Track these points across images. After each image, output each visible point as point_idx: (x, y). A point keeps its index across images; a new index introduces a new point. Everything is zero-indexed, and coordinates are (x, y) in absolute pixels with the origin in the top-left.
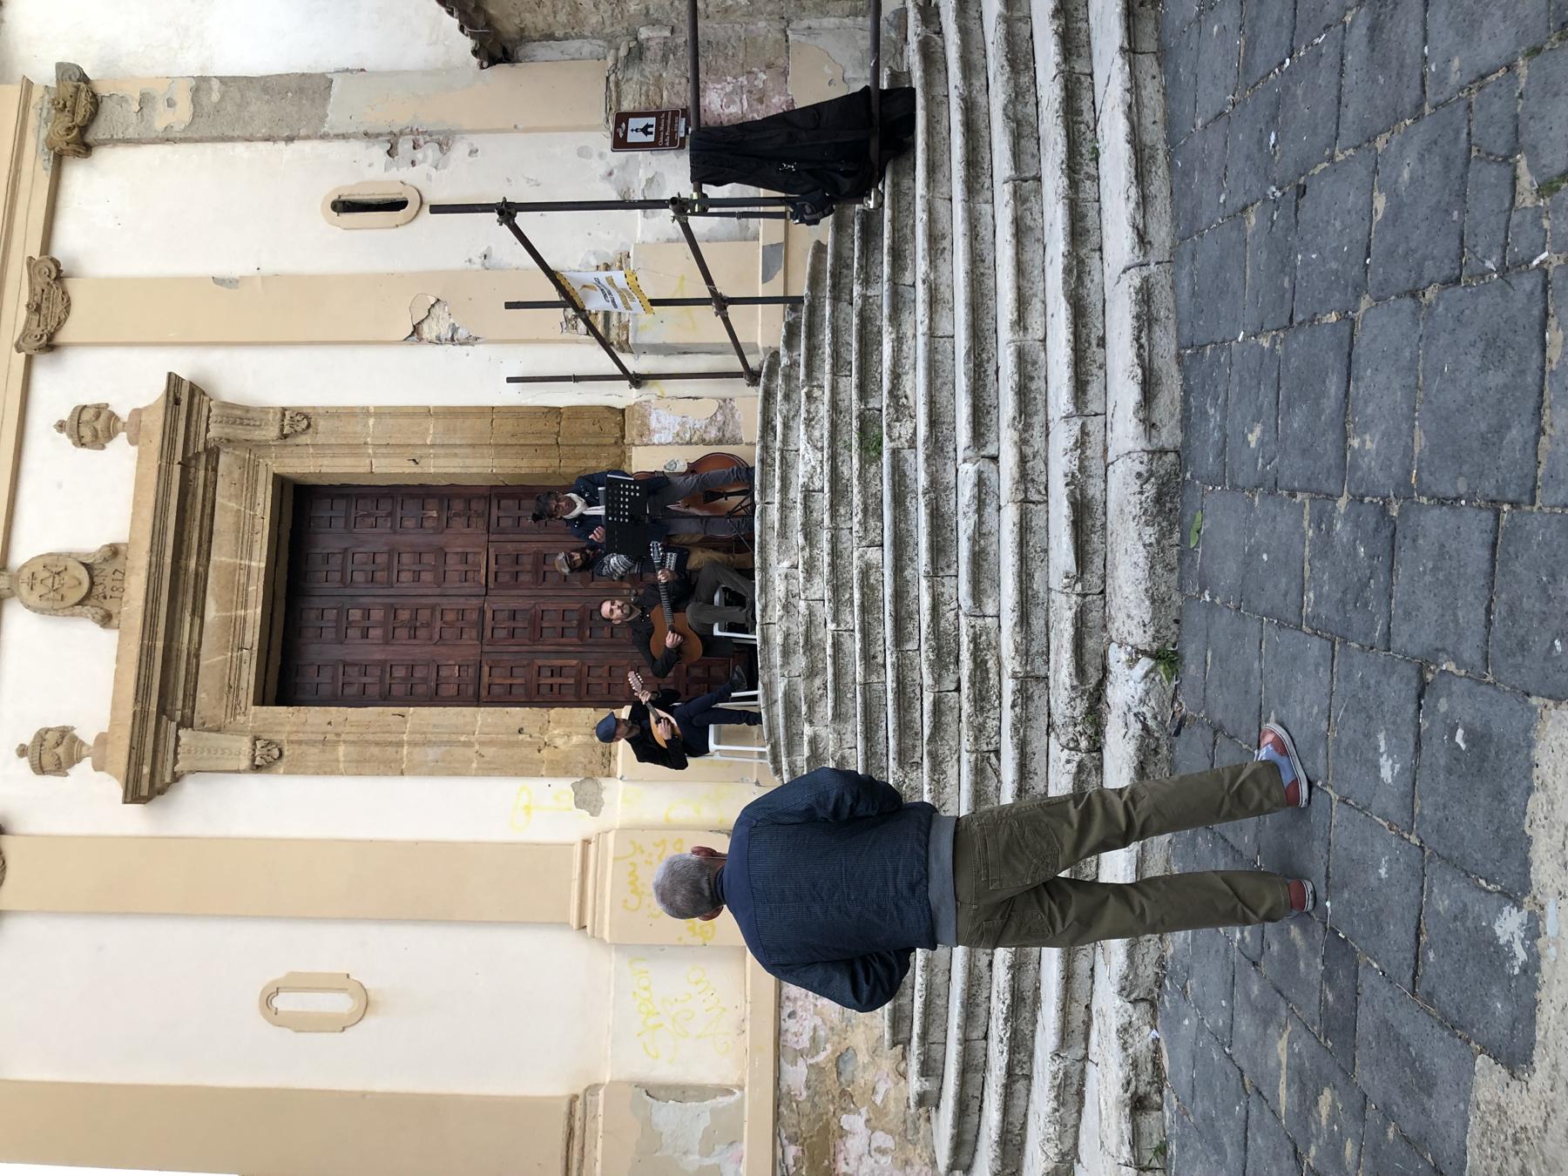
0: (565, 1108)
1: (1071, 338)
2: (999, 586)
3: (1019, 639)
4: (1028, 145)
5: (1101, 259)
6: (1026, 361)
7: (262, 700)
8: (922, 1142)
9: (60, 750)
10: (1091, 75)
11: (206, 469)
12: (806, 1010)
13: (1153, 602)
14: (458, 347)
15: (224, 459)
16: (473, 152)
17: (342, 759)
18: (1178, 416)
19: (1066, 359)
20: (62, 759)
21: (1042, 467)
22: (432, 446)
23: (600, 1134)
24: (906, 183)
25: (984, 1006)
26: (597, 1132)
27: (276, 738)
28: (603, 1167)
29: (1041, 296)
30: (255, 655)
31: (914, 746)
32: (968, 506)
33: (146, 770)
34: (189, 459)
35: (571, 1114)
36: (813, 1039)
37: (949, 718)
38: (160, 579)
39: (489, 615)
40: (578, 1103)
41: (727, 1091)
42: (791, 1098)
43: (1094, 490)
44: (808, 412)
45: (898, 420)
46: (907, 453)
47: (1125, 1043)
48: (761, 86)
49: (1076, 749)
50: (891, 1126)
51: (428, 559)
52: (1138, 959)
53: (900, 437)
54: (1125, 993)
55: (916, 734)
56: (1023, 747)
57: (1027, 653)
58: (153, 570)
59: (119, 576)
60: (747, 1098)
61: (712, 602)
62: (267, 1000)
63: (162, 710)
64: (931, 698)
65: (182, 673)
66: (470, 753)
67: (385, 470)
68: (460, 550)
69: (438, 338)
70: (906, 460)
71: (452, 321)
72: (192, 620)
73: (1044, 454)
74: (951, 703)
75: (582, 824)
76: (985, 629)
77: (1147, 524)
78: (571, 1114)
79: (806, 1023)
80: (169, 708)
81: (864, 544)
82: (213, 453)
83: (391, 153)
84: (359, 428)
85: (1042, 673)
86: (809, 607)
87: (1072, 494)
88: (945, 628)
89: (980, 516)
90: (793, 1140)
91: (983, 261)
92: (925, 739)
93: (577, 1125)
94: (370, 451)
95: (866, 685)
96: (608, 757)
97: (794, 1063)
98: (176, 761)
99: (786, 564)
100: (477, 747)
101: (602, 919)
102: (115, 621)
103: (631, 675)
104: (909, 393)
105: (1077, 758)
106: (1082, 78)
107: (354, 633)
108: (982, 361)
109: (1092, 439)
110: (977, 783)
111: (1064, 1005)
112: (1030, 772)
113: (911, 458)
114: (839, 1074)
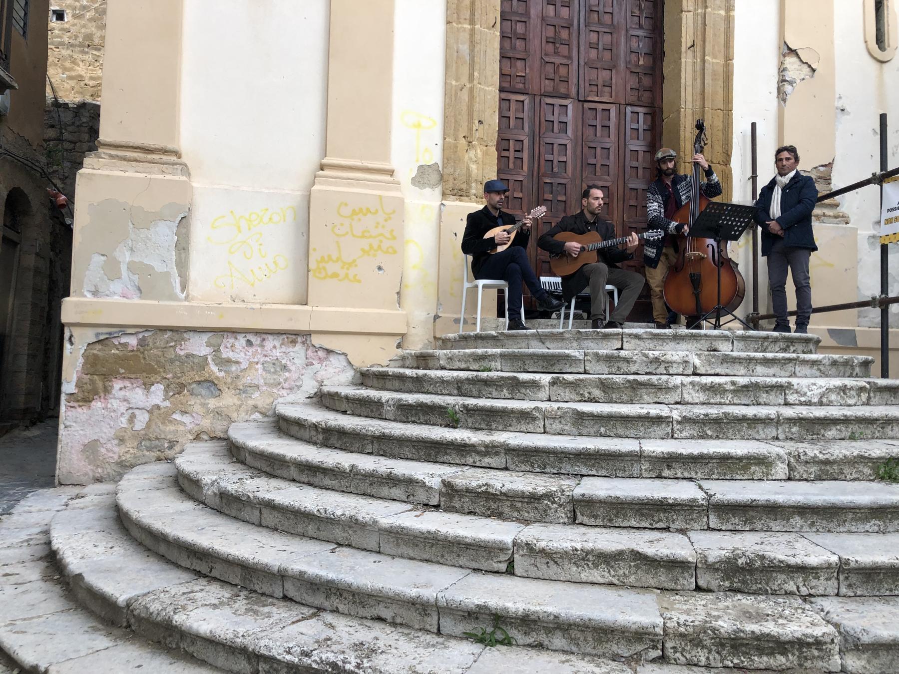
0: (170, 146)
8: (140, 453)
12: (254, 355)
14: (776, 86)
22: (704, 61)
23: (149, 176)
25: (326, 604)
26: (150, 173)
28: (119, 177)
36: (229, 361)
39: (564, 102)
40: (175, 158)
41: (184, 287)
42: (179, 342)
44: (851, 388)
50: (153, 427)
60: (179, 303)
61: (608, 284)
66: (464, 80)
67: (684, 21)
68: (614, 81)
69: (785, 70)
71: (798, 81)
74: (682, 581)
78: (165, 152)
79: (242, 354)
81: (792, 460)
86: (675, 387)
88: (775, 579)
90: (142, 343)
93: (156, 157)
94: (700, 11)
96: (461, 194)
97: (208, 345)
100: (468, 86)
101: (330, 184)
110: (623, 632)
114: (199, 383)
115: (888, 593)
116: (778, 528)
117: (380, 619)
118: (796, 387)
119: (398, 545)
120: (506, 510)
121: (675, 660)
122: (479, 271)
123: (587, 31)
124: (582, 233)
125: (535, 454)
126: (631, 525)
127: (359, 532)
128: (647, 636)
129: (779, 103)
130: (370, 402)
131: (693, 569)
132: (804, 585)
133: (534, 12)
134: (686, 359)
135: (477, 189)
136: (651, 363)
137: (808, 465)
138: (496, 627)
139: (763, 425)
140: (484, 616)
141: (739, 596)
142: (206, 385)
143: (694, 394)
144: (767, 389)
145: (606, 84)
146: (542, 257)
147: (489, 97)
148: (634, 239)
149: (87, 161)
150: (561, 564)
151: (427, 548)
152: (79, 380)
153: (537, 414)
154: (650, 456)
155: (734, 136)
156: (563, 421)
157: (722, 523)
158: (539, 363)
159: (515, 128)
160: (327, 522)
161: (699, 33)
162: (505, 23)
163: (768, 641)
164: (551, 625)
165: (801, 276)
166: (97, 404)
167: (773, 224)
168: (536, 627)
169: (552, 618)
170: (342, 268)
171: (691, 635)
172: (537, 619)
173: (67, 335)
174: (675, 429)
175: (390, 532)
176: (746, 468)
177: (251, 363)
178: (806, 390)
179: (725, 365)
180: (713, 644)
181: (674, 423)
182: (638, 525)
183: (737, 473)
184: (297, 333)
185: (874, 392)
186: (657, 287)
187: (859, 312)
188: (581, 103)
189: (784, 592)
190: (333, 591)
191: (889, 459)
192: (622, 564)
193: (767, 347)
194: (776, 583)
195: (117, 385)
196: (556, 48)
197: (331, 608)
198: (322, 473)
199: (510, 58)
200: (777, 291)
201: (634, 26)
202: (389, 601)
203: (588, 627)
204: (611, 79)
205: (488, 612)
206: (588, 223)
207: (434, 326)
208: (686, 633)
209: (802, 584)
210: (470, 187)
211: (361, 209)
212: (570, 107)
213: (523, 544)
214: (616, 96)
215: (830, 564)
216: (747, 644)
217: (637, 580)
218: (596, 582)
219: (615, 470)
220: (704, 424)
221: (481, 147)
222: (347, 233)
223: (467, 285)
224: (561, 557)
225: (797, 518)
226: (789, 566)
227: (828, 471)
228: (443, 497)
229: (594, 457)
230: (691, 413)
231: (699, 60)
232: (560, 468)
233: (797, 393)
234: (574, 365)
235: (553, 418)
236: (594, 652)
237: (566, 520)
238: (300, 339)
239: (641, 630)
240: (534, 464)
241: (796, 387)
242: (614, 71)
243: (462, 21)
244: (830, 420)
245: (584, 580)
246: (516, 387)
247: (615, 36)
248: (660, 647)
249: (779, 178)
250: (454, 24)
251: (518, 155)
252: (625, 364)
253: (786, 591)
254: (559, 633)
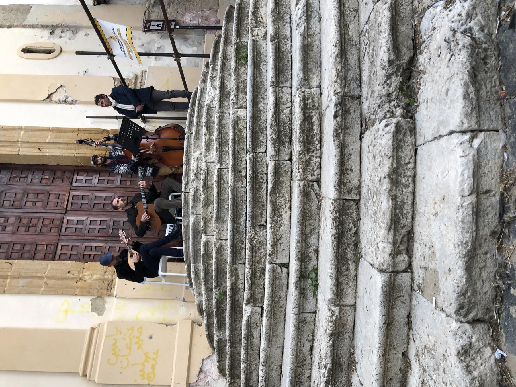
3: (339, 67)
14: (68, 105)
16: (86, 35)
22: (49, 143)
31: (262, 214)
32: (300, 18)
37: (285, 178)
44: (212, 74)
45: (256, 27)
46: (261, 42)
47: (468, 366)
48: (207, 15)
52: (475, 273)
53: (257, 35)
54: (463, 312)
55: (263, 206)
56: (342, 147)
57: (345, 78)
64: (273, 164)
66: (41, 282)
68: (56, 193)
69: (59, 101)
70: (261, 46)
71: (66, 94)
75: (94, 320)
76: (311, 95)
81: (236, 107)
83: (51, 33)
84: (16, 135)
85: (356, 93)
86: (207, 165)
88: (283, 119)
89: (308, 24)
92: (269, 191)
94: (19, 145)
95: (234, 188)
96: (111, 285)
99: (198, 153)
100: (45, 280)
101: (95, 370)
103: (121, 232)
104: (263, 16)
110: (304, 203)
111: (385, 350)
112: (347, 170)
113: (264, 45)
115: (290, 62)
116: (265, 116)
117: (311, 349)
118: (209, 102)
119: (277, 335)
120: (261, 266)
121: (318, 175)
122: (154, 274)
123: (25, 207)
124: (137, 212)
125: (235, 247)
126: (265, 194)
127: (272, 360)
128: (306, 190)
129: (78, 104)
130: (219, 347)
131: (279, 162)
132: (286, 104)
133: (8, 238)
134: (196, 159)
135: (108, 275)
136: (197, 178)
137: (239, 98)
138: (308, 277)
139: (223, 120)
140: (302, 285)
141: (293, 138)
143: (211, 155)
144: (209, 117)
145: (58, 197)
146: (156, 235)
147: (54, 267)
148: (142, 183)
150: (280, 236)
151: (277, 317)
153: (219, 244)
154: (234, 182)
155: (93, 127)
156: (222, 229)
157: (263, 145)
158: (199, 241)
159: (77, 251)
160: (268, 381)
161: (32, 145)
162: (13, 257)
163: (304, 126)
164: (304, 244)
165: (167, 95)
167: (138, 109)
168: (306, 253)
169: (299, 244)
170: (148, 362)
171: (304, 166)
172: (300, 253)
174: (225, 167)
175: (269, 340)
178: (211, 97)
179: (200, 138)
180: (308, 154)
181: (221, 167)
182: (265, 191)
183: (243, 135)
186: (172, 170)
187: (175, 67)
188: (67, 212)
189: (290, 115)
190: (297, 380)
191: (236, 58)
192: (278, 201)
194: (285, 119)
196: (33, 226)
197: (309, 381)
198: (249, 382)
199: (35, 253)
200: (175, 107)
201: (26, 181)
202: (299, 344)
203: (303, 223)
205: (298, 282)
206: (133, 208)
207: (189, 302)
208: (302, 168)
209: (286, 106)
210: (107, 279)
211: (113, 350)
212: (69, 218)
213: (270, 258)
214: (65, 191)
215: (274, 91)
216: (307, 136)
217: (287, 193)
218: (289, 216)
219: (243, 201)
220: (222, 152)
221: (84, 272)
222: (127, 359)
223: (163, 282)
224: (276, 235)
225: (260, 106)
226: (275, 112)
227: (242, 88)
228: (256, 305)
229: (235, 213)
230: (216, 158)
231: (48, 146)
232: (243, 232)
233: (212, 101)
234: (199, 220)
235: (220, 234)
236: (317, 220)
237: (265, 231)
239: (302, 193)
240: (241, 247)
241: (209, 102)
242: (51, 193)
243: (4, 284)
244: (221, 86)
245: (289, 223)
246: (207, 255)
247: (30, 192)
248: (312, 183)
249: (112, 105)
250: (6, 289)
251: (93, 249)
252: (198, 192)
253: (290, 114)
254: (309, 240)
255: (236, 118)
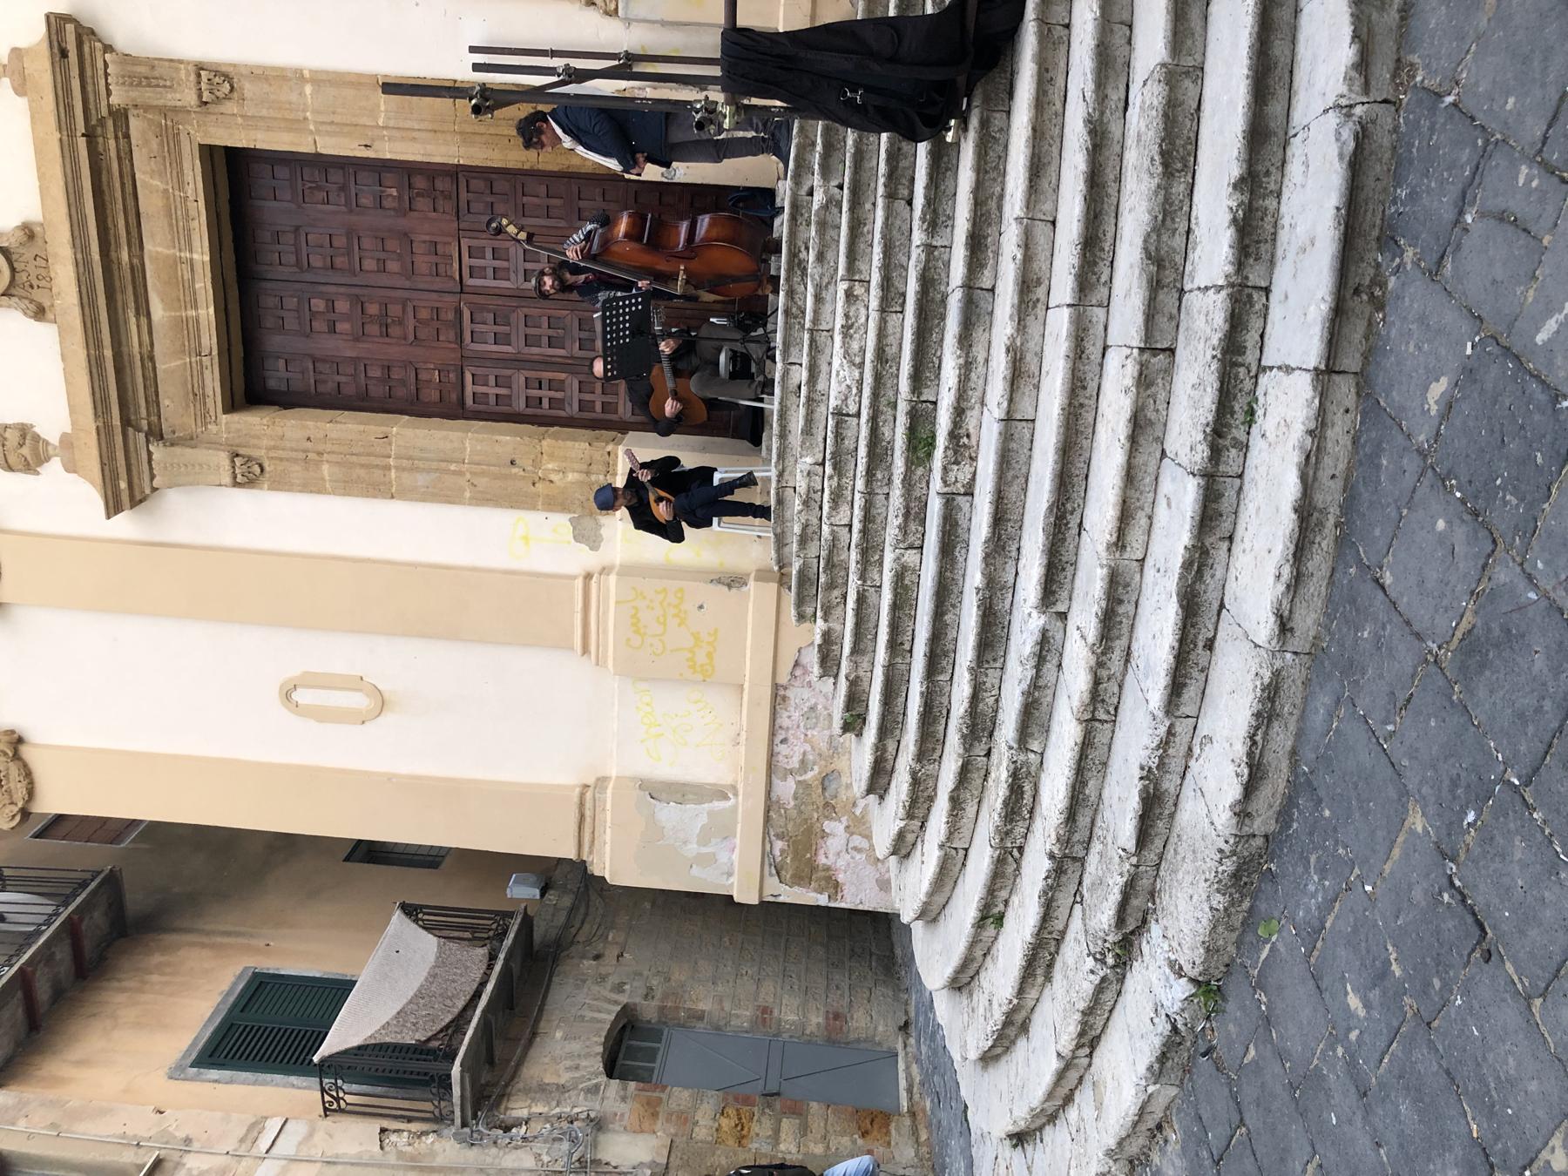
0: (576, 800)
1: (1176, 645)
2: (1047, 731)
3: (1061, 832)
4: (1167, 299)
5: (1229, 550)
6: (1118, 583)
7: (231, 406)
9: (25, 451)
10: (1267, 291)
11: (116, 138)
13: (1208, 950)
15: (135, 125)
17: (327, 478)
18: (1276, 807)
19: (1165, 666)
20: (29, 458)
21: (1116, 689)
23: (608, 824)
24: (998, 120)
27: (255, 453)
29: (1148, 510)
30: (216, 360)
33: (123, 485)
34: (94, 127)
35: (582, 804)
36: (803, 762)
38: (91, 272)
43: (1169, 784)
44: (847, 316)
45: (957, 463)
49: (1103, 962)
51: (391, 244)
58: (81, 269)
59: (40, 262)
62: (287, 695)
63: (126, 422)
65: (140, 380)
66: (462, 481)
68: (427, 238)
72: (138, 320)
73: (1120, 678)
74: (980, 765)
76: (1027, 763)
77: (1218, 891)
78: (582, 804)
80: (133, 417)
82: (120, 116)
84: (294, 97)
86: (833, 533)
87: (1145, 789)
90: (780, 837)
91: (1084, 388)
93: (588, 813)
94: (312, 127)
98: (152, 477)
102: (50, 316)
104: (972, 431)
105: (1102, 973)
106: (1255, 296)
107: (319, 325)
108: (1065, 512)
109: (1177, 740)
114: (824, 789)
118: (839, 402)
142: (826, 783)
149: (597, 873)
152: (815, 891)
166: (841, 877)
173: (772, 899)
176: (906, 588)
177: (805, 741)
179: (814, 431)
184: (775, 696)
185: (854, 274)
193: (799, 308)
195: (822, 860)
204: (424, 242)
238: (781, 692)
241: (839, 402)
251: (545, 384)
255: (899, 568)
